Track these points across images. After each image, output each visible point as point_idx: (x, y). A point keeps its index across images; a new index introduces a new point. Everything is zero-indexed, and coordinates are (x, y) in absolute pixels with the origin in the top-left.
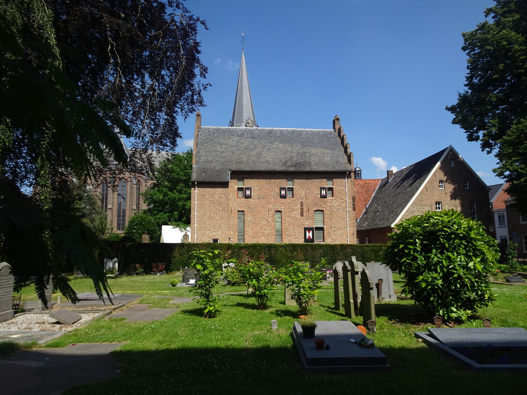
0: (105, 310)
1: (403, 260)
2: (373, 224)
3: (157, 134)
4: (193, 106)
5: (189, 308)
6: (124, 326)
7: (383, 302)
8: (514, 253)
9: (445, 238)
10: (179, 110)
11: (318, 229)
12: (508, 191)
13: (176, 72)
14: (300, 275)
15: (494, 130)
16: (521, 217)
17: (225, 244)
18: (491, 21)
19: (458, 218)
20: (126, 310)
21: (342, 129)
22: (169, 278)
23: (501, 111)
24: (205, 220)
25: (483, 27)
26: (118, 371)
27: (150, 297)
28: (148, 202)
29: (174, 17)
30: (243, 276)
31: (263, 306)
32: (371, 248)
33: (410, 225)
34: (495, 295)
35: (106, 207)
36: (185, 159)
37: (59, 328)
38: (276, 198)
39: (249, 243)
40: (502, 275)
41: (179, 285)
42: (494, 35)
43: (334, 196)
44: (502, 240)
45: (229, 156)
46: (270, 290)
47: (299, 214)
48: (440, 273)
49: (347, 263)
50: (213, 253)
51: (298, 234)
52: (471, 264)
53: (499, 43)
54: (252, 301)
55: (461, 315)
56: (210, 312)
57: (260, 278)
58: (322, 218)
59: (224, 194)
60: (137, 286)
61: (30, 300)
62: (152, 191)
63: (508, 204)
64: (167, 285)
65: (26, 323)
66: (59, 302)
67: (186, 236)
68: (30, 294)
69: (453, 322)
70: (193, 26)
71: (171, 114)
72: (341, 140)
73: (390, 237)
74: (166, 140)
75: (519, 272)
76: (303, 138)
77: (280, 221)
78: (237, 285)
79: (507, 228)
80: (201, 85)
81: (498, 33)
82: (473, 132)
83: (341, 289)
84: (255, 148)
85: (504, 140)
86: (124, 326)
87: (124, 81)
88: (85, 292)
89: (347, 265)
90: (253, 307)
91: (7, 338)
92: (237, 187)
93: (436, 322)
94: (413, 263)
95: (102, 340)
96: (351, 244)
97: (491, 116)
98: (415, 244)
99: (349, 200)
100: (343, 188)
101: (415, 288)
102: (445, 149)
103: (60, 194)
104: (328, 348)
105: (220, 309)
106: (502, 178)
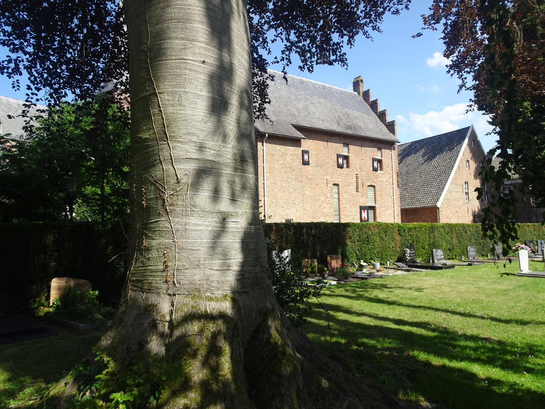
24: (276, 192)
77: (337, 197)
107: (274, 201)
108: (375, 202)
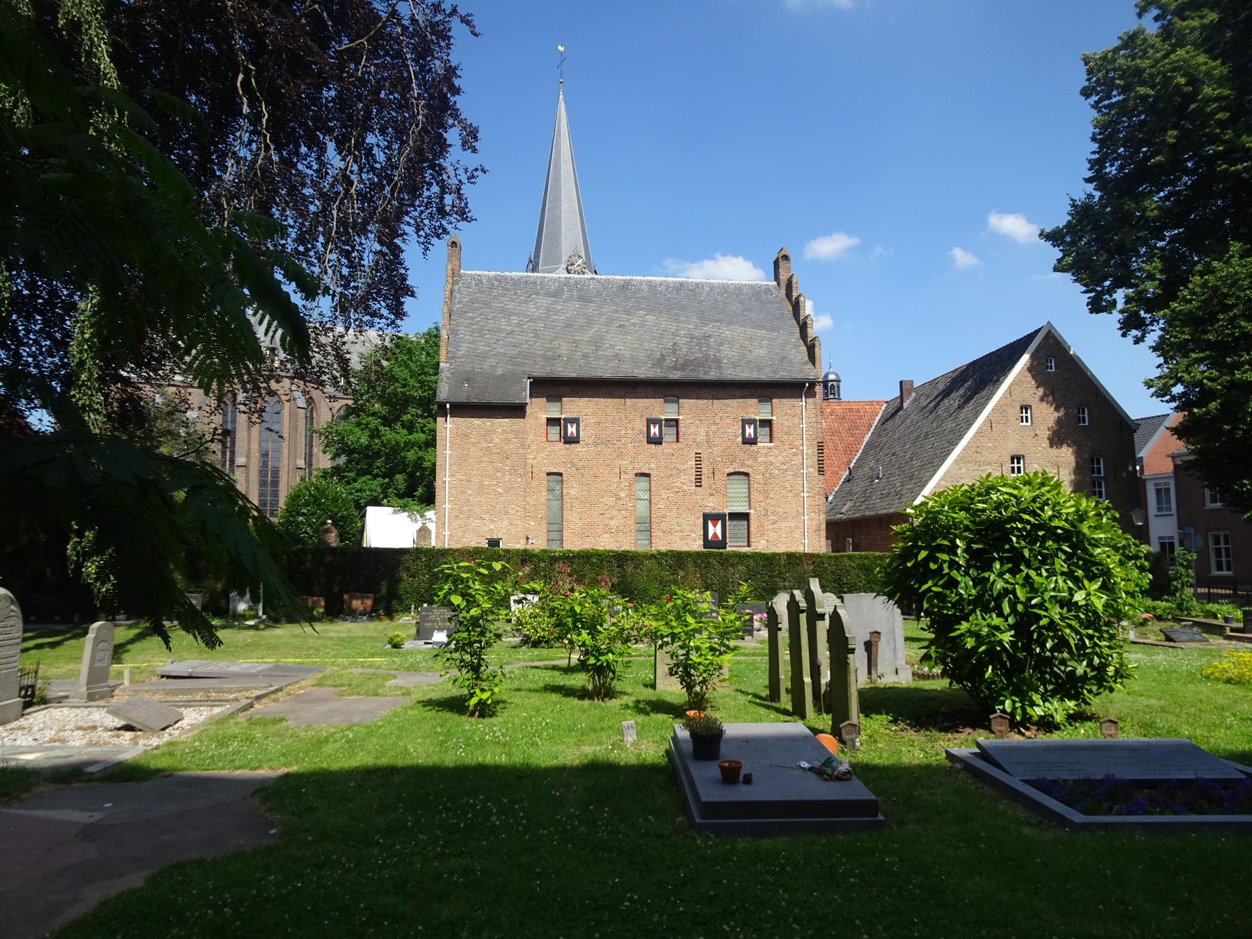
0: (237, 700)
1: (925, 587)
2: (864, 507)
3: (356, 288)
4: (444, 222)
5: (434, 696)
6: (282, 736)
7: (881, 683)
8: (1188, 576)
9: (1024, 538)
10: (410, 230)
11: (735, 516)
12: (1180, 432)
13: (401, 139)
14: (690, 619)
15: (1151, 288)
16: (1207, 492)
17: (517, 551)
18: (1151, 27)
19: (1054, 492)
20: (285, 701)
21: (794, 280)
22: (384, 629)
23: (1169, 243)
24: (470, 495)
25: (1131, 41)
26: (272, 832)
27: (342, 672)
28: (334, 450)
29: (395, 5)
30: (559, 624)
31: (606, 693)
32: (858, 561)
33: (943, 506)
34: (1130, 666)
35: (232, 461)
36: (423, 349)
37: (131, 740)
38: (636, 445)
39: (573, 549)
40: (1156, 626)
41: (407, 645)
42: (1157, 61)
43: (775, 440)
44: (1163, 545)
45: (527, 342)
46: (621, 654)
47: (691, 481)
48: (1009, 615)
49: (797, 593)
50: (489, 568)
51: (689, 528)
52: (1079, 597)
53: (1167, 80)
54: (580, 680)
55: (1052, 711)
56: (481, 703)
57: (598, 627)
58: (746, 490)
59: (516, 433)
60: (310, 648)
61: (58, 677)
62: (343, 426)
63: (1179, 462)
64: (379, 645)
65: (51, 729)
66: (126, 682)
67: (423, 532)
68: (57, 665)
69: (1035, 728)
70: (441, 28)
71: (390, 237)
72: (793, 306)
73: (898, 533)
74: (379, 302)
75: (1196, 619)
76: (703, 301)
78: (543, 644)
79: (1175, 517)
80: (461, 172)
81: (1166, 56)
82: (1102, 293)
83: (785, 655)
84: (590, 323)
85: (1173, 311)
86: (282, 736)
87: (275, 158)
88: (186, 659)
89: (797, 598)
90: (583, 694)
91: (13, 759)
92: (545, 416)
93: (995, 727)
94: (948, 592)
95: (233, 765)
96: (811, 552)
97: (1143, 255)
98: (952, 549)
99: (809, 451)
100: (796, 420)
101: (951, 649)
102: (1037, 332)
103: (123, 427)
104: (748, 780)
105: (504, 697)
106: (1167, 401)
107: (466, 509)
108: (749, 505)
